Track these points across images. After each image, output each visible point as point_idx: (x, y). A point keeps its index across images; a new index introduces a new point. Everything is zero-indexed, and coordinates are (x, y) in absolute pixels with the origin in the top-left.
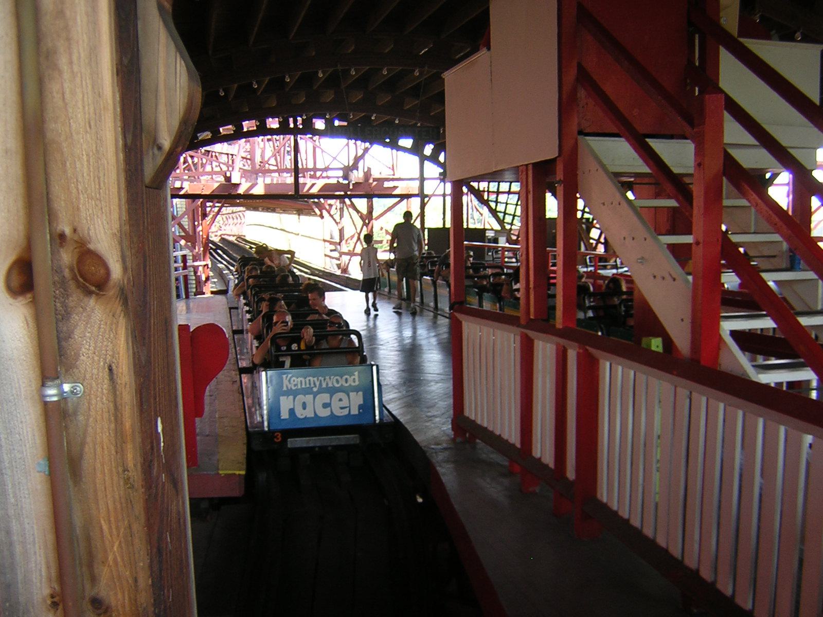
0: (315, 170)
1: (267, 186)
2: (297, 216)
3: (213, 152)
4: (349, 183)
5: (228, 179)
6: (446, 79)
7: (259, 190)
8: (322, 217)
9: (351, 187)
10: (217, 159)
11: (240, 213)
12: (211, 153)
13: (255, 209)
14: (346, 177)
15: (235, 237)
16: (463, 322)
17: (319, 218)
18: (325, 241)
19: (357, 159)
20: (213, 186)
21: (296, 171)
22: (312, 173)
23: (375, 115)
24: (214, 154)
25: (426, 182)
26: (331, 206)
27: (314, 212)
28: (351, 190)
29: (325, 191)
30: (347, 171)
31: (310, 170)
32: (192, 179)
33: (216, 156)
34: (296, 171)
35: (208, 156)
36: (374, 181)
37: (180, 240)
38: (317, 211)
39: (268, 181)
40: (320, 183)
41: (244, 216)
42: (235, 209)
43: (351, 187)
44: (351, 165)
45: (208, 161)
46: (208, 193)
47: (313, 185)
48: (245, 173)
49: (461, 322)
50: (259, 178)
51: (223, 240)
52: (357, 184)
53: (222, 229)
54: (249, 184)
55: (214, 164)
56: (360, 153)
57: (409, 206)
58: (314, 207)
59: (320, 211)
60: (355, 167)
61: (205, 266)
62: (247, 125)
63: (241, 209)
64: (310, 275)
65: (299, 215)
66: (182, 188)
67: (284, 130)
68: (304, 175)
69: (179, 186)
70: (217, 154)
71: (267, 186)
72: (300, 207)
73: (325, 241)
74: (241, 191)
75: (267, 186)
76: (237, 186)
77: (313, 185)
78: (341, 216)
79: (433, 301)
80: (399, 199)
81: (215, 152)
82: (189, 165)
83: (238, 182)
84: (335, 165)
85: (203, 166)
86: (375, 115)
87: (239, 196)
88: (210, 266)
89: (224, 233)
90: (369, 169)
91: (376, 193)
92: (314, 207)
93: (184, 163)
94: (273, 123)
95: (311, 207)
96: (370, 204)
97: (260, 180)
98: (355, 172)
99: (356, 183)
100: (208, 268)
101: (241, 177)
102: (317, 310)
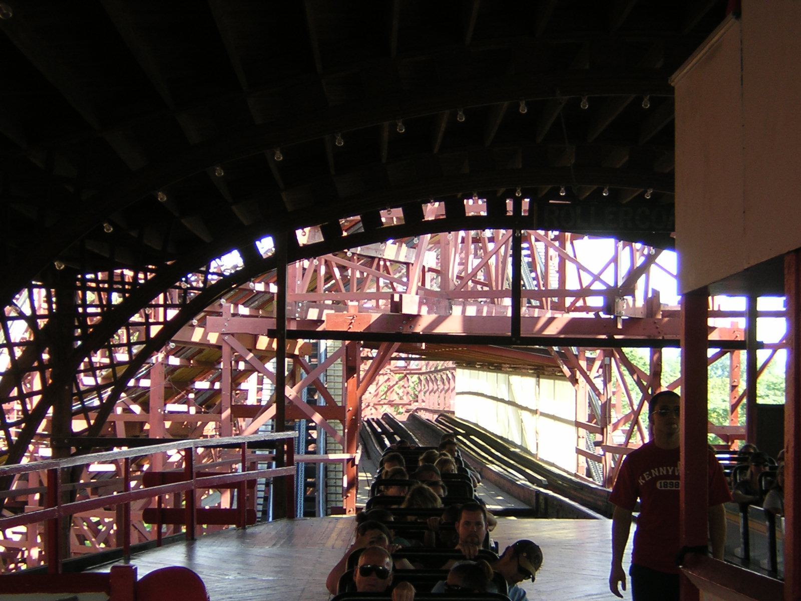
0: (562, 292)
1: (467, 321)
2: (532, 380)
3: (380, 259)
4: (616, 318)
5: (397, 306)
6: (676, 88)
7: (452, 326)
8: (575, 381)
9: (620, 326)
10: (388, 273)
11: (448, 372)
12: (376, 261)
13: (470, 364)
14: (609, 308)
15: (436, 416)
16: (701, 592)
17: (569, 384)
18: (578, 425)
19: (634, 274)
20: (370, 317)
21: (517, 292)
22: (556, 299)
23: (650, 191)
24: (382, 263)
25: (759, 320)
26: (591, 361)
27: (562, 372)
28: (620, 332)
29: (572, 333)
30: (613, 295)
31: (553, 293)
32: (339, 305)
33: (385, 266)
34: (517, 292)
35: (371, 267)
36: (663, 316)
37: (313, 414)
38: (565, 369)
39: (471, 311)
40: (563, 319)
41: (454, 377)
42: (440, 364)
43: (620, 326)
44: (620, 284)
45: (371, 276)
46: (360, 329)
47: (551, 320)
48: (427, 297)
49: (698, 590)
50: (453, 307)
51: (414, 419)
52: (632, 322)
53: (420, 399)
54: (433, 316)
55: (382, 281)
56: (640, 261)
57: (735, 364)
58: (560, 362)
59: (571, 369)
60: (628, 288)
61: (348, 460)
62: (433, 210)
63: (450, 364)
64: (546, 487)
65: (538, 377)
66: (320, 321)
67: (495, 219)
68: (541, 302)
69: (315, 318)
70: (388, 264)
71: (467, 320)
72: (538, 362)
73: (578, 425)
74: (419, 329)
75: (467, 321)
76: (413, 319)
77: (551, 320)
78: (607, 379)
79: (742, 546)
80: (718, 350)
81: (385, 260)
82: (337, 280)
83: (414, 312)
84: (597, 286)
85: (361, 282)
86: (650, 191)
87: (419, 338)
88: (357, 462)
89: (423, 405)
90: (656, 294)
91: (668, 337)
92: (560, 362)
93: (327, 280)
94: (475, 206)
95: (555, 362)
96: (656, 356)
97: (457, 310)
98: (629, 298)
99: (631, 319)
100: (353, 464)
101: (421, 304)
102: (459, 551)
